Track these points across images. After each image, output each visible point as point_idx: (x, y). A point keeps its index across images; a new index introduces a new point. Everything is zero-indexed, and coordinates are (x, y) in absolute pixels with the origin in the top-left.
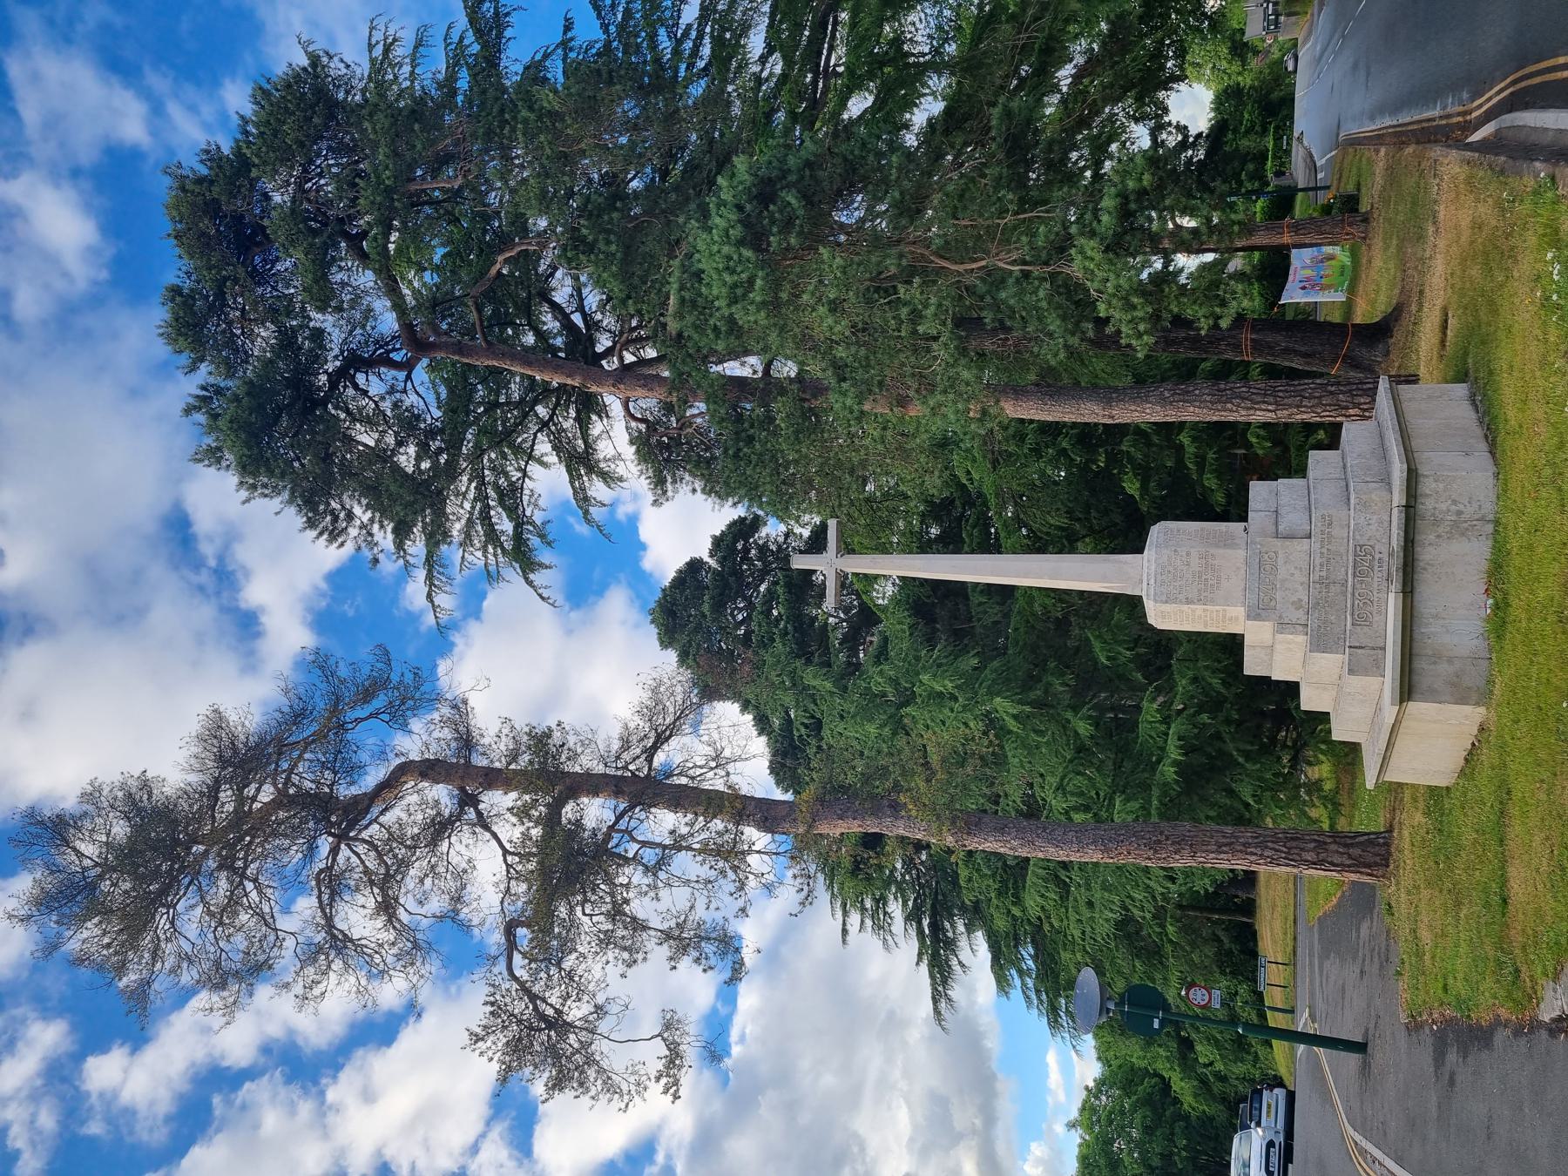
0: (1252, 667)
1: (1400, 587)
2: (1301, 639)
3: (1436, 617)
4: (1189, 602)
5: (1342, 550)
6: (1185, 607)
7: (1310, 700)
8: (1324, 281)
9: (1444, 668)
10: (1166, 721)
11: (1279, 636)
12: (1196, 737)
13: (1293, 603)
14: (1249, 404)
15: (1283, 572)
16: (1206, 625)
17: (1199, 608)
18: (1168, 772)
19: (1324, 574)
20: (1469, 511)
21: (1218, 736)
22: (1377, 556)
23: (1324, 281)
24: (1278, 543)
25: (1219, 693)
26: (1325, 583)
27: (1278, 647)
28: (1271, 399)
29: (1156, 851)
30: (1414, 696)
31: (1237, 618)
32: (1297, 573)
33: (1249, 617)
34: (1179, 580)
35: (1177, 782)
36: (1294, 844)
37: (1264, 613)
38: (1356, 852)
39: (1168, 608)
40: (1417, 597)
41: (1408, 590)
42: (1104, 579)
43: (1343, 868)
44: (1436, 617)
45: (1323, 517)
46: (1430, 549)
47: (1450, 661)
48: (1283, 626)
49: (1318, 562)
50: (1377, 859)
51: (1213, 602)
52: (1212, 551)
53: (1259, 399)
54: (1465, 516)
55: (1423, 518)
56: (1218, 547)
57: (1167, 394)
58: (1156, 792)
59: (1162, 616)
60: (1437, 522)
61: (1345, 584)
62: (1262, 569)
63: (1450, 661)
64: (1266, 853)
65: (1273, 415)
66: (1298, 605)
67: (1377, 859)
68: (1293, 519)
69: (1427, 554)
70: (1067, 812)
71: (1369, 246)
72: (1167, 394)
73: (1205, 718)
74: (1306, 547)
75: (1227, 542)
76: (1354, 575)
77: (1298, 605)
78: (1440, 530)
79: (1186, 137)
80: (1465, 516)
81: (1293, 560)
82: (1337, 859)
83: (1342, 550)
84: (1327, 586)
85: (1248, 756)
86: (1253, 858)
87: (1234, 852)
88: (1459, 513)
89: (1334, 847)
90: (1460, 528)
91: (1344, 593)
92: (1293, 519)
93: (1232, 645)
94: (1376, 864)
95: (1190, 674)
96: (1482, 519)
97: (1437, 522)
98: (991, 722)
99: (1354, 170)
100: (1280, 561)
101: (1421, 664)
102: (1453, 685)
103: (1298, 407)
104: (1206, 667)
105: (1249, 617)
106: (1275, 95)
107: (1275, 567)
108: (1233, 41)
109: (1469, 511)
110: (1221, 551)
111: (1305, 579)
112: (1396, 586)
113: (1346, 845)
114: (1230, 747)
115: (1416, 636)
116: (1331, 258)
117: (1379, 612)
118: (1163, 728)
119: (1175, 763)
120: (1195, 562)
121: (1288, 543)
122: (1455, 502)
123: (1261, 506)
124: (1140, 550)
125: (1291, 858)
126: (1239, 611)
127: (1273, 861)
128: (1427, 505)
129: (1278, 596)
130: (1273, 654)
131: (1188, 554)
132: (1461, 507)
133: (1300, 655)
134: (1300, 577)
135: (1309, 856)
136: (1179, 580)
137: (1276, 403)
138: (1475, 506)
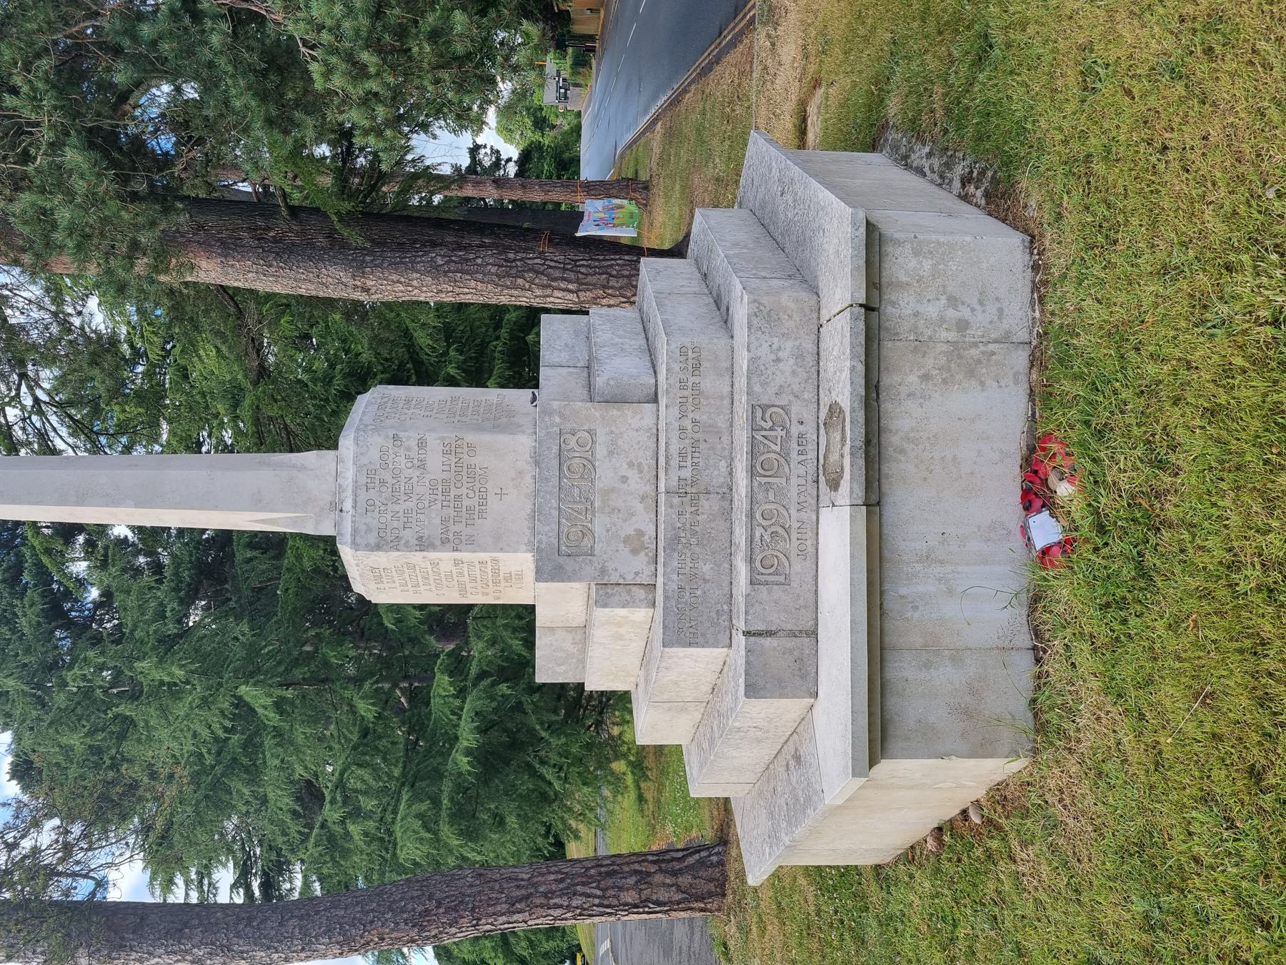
0: (550, 668)
1: (860, 493)
2: (641, 614)
3: (927, 558)
4: (423, 544)
5: (721, 422)
6: (417, 557)
7: (648, 727)
8: (616, 221)
9: (946, 677)
10: (462, 693)
11: (601, 613)
12: (495, 711)
13: (627, 540)
14: (544, 280)
15: (605, 474)
16: (463, 591)
17: (445, 558)
18: (461, 761)
19: (687, 473)
20: (981, 320)
21: (519, 707)
22: (795, 430)
23: (616, 221)
24: (596, 411)
25: (520, 655)
26: (689, 492)
27: (598, 633)
28: (572, 276)
29: (422, 929)
30: (893, 745)
31: (520, 576)
32: (633, 474)
33: (540, 575)
34: (416, 506)
35: (469, 773)
36: (610, 882)
37: (570, 565)
38: (685, 880)
39: (382, 559)
40: (890, 513)
41: (873, 501)
42: (257, 503)
43: (671, 906)
44: (927, 558)
45: (683, 351)
46: (910, 405)
47: (957, 657)
48: (608, 591)
49: (674, 449)
50: (711, 886)
51: (471, 543)
52: (470, 437)
53: (557, 274)
54: (974, 333)
55: (895, 336)
56: (479, 428)
57: (440, 261)
58: (447, 786)
59: (383, 577)
60: (921, 345)
61: (727, 494)
62: (565, 467)
63: (957, 657)
64: (574, 903)
65: (573, 297)
66: (635, 543)
67: (711, 886)
68: (620, 365)
69: (903, 418)
70: (343, 822)
71: (650, 212)
72: (440, 261)
73: (504, 688)
74: (649, 421)
75: (501, 422)
76: (752, 473)
77: (635, 543)
78: (929, 362)
79: (498, 159)
80: (974, 333)
81: (625, 452)
82: (663, 895)
83: (721, 422)
84: (695, 501)
85: (550, 727)
86: (557, 912)
87: (531, 908)
88: (962, 326)
89: (658, 878)
90: (965, 363)
91: (727, 514)
92: (620, 365)
93: (522, 619)
94: (711, 894)
95: (488, 634)
96: (1005, 339)
97: (921, 345)
98: (243, 710)
99: (632, 164)
100: (601, 451)
101: (903, 669)
102: (968, 714)
103: (604, 287)
104: (506, 626)
105: (540, 575)
106: (566, 155)
107: (590, 463)
108: (536, 117)
109: (981, 320)
110: (486, 438)
111: (649, 489)
112: (850, 488)
113: (675, 873)
114: (532, 720)
115: (888, 605)
116: (622, 207)
117: (802, 553)
118: (457, 703)
119: (468, 752)
120: (435, 461)
121: (614, 412)
122: (953, 301)
123: (563, 357)
124: (331, 443)
125: (610, 906)
126: (523, 561)
127: (584, 912)
128: (903, 307)
129: (598, 528)
130: (590, 642)
131: (422, 444)
132: (965, 313)
133: (637, 646)
134: (638, 484)
135: (629, 897)
136: (416, 506)
137: (578, 281)
138: (992, 309)
